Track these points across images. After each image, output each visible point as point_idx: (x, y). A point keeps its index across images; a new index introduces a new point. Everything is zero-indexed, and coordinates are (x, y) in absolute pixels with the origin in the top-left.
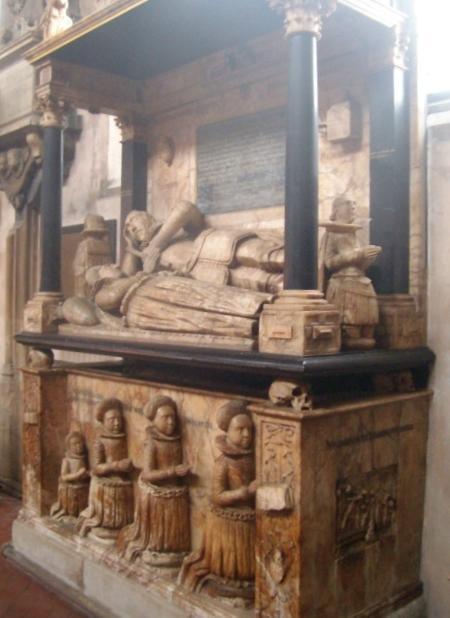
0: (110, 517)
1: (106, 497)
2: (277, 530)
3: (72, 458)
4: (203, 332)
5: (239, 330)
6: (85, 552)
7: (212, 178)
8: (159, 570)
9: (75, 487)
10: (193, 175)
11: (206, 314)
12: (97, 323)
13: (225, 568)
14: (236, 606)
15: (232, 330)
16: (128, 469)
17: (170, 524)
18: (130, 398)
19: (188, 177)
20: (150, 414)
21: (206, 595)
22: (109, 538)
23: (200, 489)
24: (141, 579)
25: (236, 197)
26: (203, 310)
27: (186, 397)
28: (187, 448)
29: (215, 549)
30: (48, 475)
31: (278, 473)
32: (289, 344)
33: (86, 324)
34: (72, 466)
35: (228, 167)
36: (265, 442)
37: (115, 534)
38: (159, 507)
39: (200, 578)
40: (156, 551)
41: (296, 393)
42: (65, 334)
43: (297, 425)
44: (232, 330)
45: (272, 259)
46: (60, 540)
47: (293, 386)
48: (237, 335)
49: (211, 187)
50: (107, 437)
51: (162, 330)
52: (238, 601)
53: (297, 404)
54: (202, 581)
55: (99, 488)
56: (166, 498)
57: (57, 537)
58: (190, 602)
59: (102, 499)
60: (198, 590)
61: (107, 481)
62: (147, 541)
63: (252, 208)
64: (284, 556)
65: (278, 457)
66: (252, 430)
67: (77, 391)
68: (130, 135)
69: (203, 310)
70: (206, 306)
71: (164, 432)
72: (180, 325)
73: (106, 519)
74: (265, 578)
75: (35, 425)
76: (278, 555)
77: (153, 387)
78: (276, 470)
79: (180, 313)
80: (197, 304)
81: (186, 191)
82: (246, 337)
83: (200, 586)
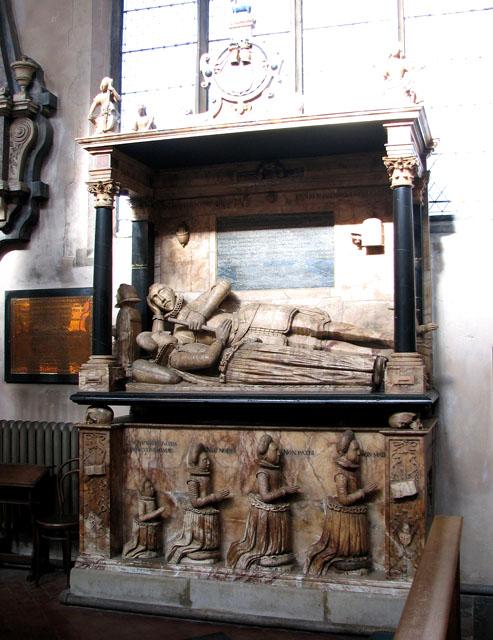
0: (211, 540)
1: (207, 524)
2: (404, 510)
3: (148, 500)
6: (187, 575)
7: (234, 261)
8: (279, 568)
9: (155, 524)
10: (213, 256)
11: (325, 371)
12: (181, 380)
14: (362, 575)
17: (285, 531)
18: (214, 441)
19: (208, 257)
21: (334, 574)
23: (300, 502)
24: (263, 579)
25: (262, 279)
26: (323, 368)
27: (284, 434)
28: (286, 473)
30: (116, 520)
32: (412, 387)
33: (171, 383)
35: (253, 254)
36: (391, 454)
40: (274, 554)
41: (414, 419)
43: (108, 433)
44: (354, 381)
45: (326, 329)
46: (149, 573)
47: (413, 415)
48: (358, 384)
49: (234, 268)
50: (201, 475)
51: (276, 384)
52: (363, 570)
53: (414, 425)
54: (328, 565)
55: (200, 518)
57: (146, 572)
58: (322, 582)
59: (203, 527)
60: (324, 573)
61: (203, 511)
62: (266, 549)
63: (280, 288)
64: (410, 526)
65: (404, 462)
68: (145, 216)
69: (323, 368)
70: (324, 364)
71: (273, 463)
72: (299, 379)
73: (208, 542)
74: (393, 546)
76: (406, 527)
77: (244, 429)
78: (402, 471)
79: (297, 371)
80: (316, 364)
81: (205, 269)
82: (367, 385)
83: (325, 569)
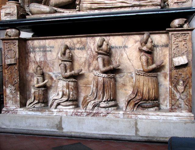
0: (73, 95)
4: (133, 6)
5: (154, 3)
8: (110, 109)
9: (43, 89)
13: (150, 96)
15: (151, 3)
16: (77, 74)
20: (99, 44)
22: (72, 105)
24: (101, 114)
28: (112, 59)
29: (145, 89)
31: (180, 52)
34: (39, 80)
36: (173, 42)
37: (75, 103)
38: (108, 82)
39: (136, 104)
42: (29, 18)
44: (151, 3)
46: (40, 114)
47: (185, 19)
56: (111, 78)
58: (134, 114)
65: (180, 46)
66: (88, 69)
67: (34, 48)
73: (71, 96)
75: (15, 64)
76: (181, 82)
83: (135, 108)
